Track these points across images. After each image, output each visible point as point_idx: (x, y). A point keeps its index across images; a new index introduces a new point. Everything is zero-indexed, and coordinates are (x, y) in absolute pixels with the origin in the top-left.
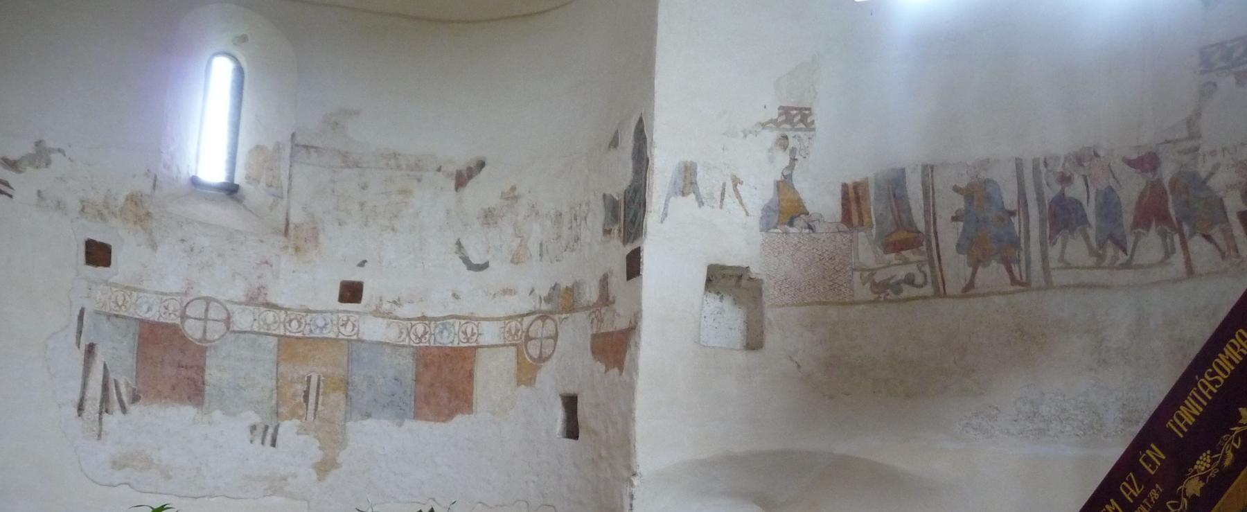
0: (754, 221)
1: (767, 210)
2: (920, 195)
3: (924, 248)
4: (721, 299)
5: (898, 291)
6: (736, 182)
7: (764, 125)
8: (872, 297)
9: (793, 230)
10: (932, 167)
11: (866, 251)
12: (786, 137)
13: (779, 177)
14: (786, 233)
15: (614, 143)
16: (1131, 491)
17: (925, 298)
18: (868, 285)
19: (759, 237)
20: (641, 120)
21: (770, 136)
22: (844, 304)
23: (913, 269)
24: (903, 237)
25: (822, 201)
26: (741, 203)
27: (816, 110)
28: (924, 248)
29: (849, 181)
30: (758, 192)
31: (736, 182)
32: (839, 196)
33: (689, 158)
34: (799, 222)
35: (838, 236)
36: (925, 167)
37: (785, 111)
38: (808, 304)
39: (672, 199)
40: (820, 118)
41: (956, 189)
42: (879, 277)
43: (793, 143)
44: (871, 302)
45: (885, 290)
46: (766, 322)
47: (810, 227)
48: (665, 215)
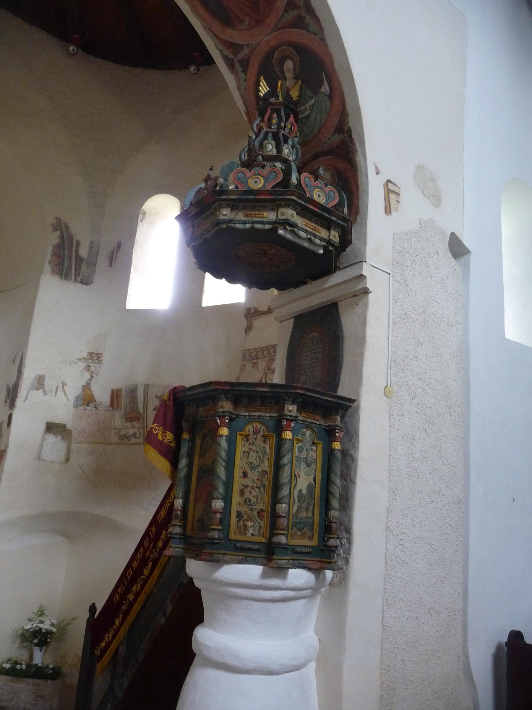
0: (71, 403)
1: (77, 398)
2: (142, 398)
3: (141, 421)
4: (56, 437)
5: (129, 440)
6: (64, 384)
7: (80, 360)
8: (118, 441)
9: (88, 408)
10: (148, 385)
11: (118, 421)
12: (89, 366)
13: (84, 384)
14: (85, 409)
15: (14, 361)
16: (146, 544)
17: (139, 444)
18: (117, 436)
19: (72, 410)
20: (23, 354)
21: (82, 365)
22: (106, 444)
23: (136, 430)
24: (133, 416)
25: (102, 396)
26: (65, 394)
27: (104, 355)
28: (141, 421)
29: (114, 388)
30: (74, 390)
31: (64, 384)
32: (110, 394)
33: (41, 373)
34: (91, 405)
35: (107, 412)
36: (145, 385)
37: (91, 354)
38: (92, 443)
39: (31, 391)
40: (105, 359)
41: (156, 396)
42: (123, 433)
43: (92, 369)
44: (118, 444)
45: (124, 438)
46: (71, 449)
47: (96, 407)
48: (26, 398)
